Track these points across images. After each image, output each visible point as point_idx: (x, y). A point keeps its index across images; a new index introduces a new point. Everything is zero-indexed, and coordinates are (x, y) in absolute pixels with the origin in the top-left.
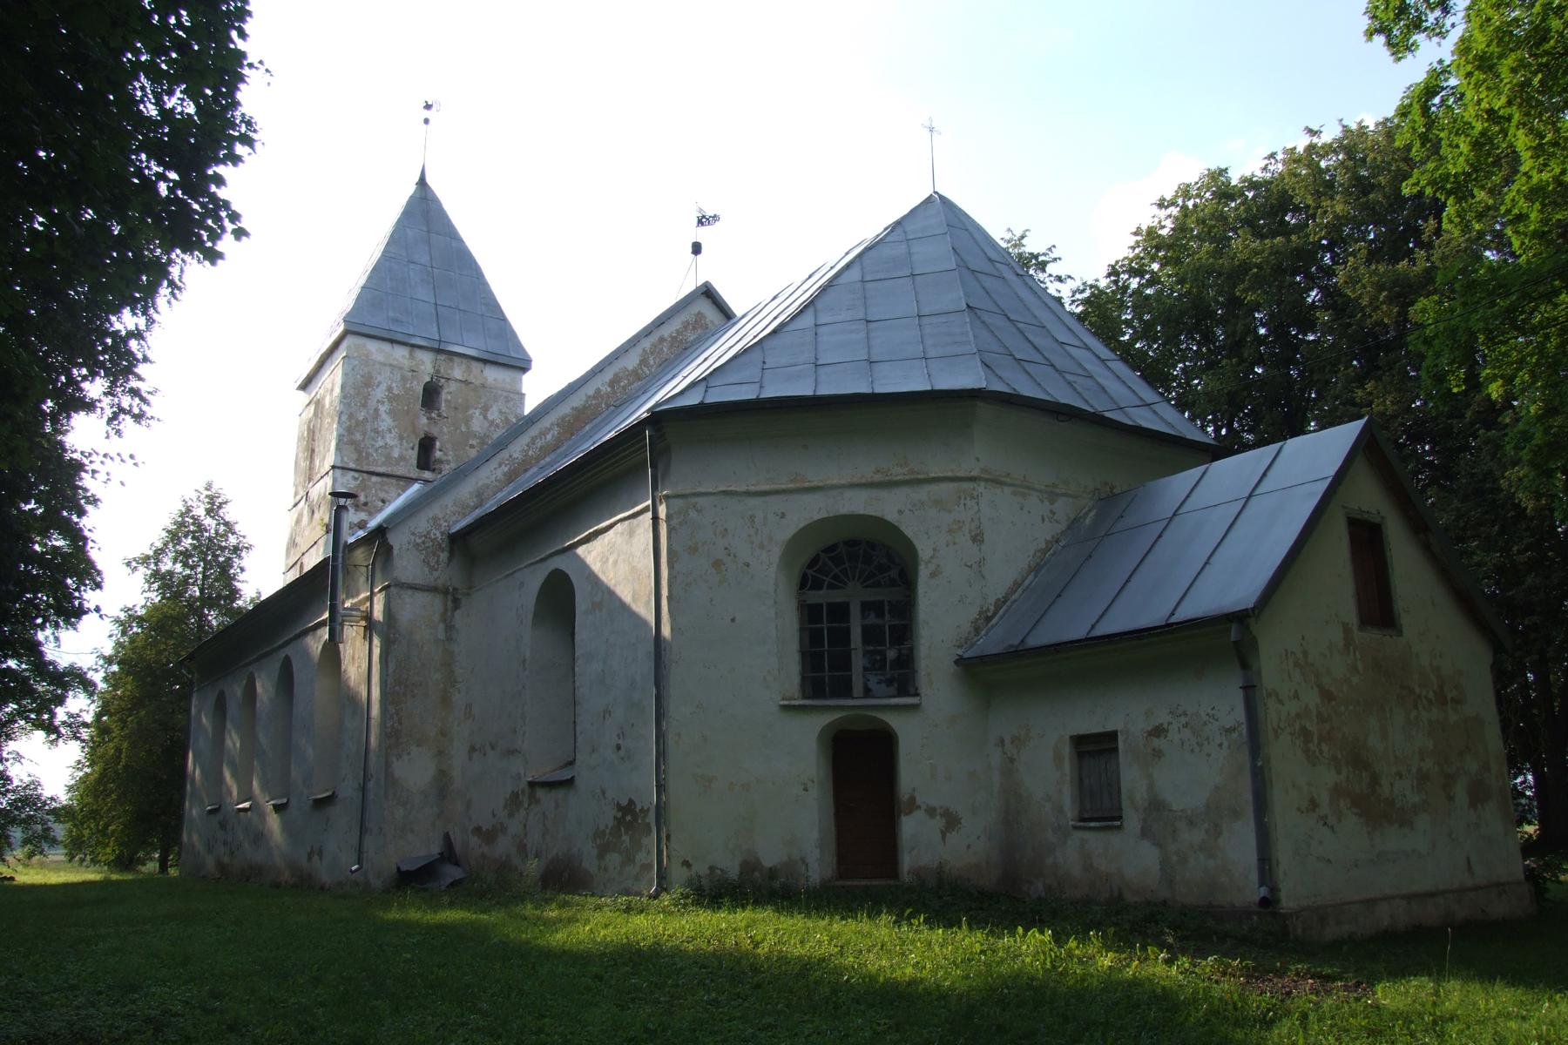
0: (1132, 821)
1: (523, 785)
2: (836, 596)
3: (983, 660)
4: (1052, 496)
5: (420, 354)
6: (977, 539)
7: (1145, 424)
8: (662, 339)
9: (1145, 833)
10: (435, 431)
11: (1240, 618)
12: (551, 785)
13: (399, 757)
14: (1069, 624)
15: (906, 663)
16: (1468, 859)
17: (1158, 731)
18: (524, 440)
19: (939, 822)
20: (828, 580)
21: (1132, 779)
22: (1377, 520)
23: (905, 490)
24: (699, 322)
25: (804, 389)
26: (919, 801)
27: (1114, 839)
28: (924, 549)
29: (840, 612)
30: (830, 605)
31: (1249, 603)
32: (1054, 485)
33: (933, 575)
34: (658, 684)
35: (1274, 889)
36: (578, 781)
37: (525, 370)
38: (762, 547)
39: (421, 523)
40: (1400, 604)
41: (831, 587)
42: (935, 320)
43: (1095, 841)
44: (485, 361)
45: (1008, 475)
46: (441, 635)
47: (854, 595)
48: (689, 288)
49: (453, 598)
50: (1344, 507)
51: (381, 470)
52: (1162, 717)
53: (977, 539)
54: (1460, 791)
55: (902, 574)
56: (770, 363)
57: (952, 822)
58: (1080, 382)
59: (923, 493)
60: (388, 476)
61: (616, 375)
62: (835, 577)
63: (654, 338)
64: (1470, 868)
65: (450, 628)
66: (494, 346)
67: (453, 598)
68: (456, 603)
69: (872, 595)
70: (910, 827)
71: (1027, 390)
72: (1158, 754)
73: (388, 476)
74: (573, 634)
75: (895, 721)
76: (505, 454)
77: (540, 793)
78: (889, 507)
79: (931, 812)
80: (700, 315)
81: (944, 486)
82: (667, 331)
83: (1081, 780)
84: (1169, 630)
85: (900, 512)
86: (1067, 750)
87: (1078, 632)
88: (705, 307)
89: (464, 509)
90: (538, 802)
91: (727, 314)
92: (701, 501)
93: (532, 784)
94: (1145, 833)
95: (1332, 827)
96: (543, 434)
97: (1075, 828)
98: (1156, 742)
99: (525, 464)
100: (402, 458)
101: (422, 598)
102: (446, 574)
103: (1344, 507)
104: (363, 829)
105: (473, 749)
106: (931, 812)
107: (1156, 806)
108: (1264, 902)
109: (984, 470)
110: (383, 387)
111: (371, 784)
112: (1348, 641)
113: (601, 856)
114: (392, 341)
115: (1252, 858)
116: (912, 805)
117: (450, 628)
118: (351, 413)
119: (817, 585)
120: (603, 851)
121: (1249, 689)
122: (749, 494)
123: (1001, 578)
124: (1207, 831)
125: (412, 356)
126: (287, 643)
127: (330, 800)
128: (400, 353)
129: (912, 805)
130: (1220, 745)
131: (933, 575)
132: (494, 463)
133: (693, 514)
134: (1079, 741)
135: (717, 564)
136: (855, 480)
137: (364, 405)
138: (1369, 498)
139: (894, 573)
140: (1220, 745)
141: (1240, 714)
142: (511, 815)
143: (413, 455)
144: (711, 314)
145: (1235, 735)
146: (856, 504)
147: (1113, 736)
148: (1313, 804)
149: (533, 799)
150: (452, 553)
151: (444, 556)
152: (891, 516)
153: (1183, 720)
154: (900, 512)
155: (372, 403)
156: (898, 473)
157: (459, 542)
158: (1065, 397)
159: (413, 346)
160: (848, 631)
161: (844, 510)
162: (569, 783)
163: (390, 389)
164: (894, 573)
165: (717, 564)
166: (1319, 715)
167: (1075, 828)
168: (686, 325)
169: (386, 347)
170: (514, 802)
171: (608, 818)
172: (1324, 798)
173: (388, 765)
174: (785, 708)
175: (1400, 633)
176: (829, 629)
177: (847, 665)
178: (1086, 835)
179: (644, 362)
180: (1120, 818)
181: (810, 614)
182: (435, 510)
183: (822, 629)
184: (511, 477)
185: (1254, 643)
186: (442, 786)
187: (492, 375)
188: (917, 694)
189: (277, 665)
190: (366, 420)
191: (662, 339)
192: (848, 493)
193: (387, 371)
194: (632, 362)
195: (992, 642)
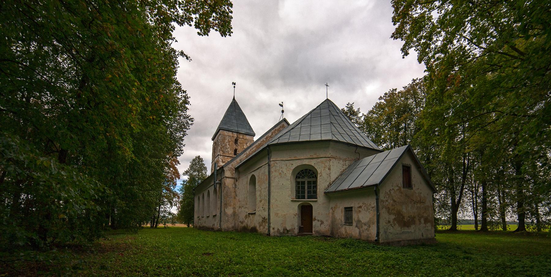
0: (354, 224)
1: (247, 214)
2: (303, 180)
3: (328, 192)
4: (345, 160)
5: (234, 133)
6: (329, 169)
7: (365, 146)
8: (276, 130)
9: (356, 226)
10: (237, 148)
11: (376, 185)
12: (252, 214)
13: (226, 208)
14: (345, 186)
15: (315, 192)
16: (422, 233)
17: (360, 207)
18: (249, 150)
19: (320, 223)
20: (301, 177)
21: (355, 216)
22: (409, 166)
23: (316, 159)
24: (283, 126)
25: (319, 138)
26: (316, 218)
27: (351, 227)
28: (319, 171)
29: (303, 183)
30: (301, 182)
31: (378, 181)
32: (346, 158)
33: (320, 176)
34: (269, 196)
35: (378, 238)
36: (256, 213)
37: (254, 136)
38: (288, 171)
39: (230, 166)
40: (413, 182)
41: (302, 178)
42: (324, 125)
43: (348, 227)
44: (246, 134)
45: (336, 157)
46: (234, 186)
47: (306, 180)
48: (281, 119)
49: (236, 180)
50: (402, 163)
51: (227, 155)
52: (361, 205)
53: (329, 169)
54: (422, 221)
55: (315, 175)
56: (292, 134)
57: (322, 223)
58: (353, 138)
59: (319, 160)
60: (229, 156)
61: (267, 137)
62: (303, 176)
63: (274, 130)
64: (423, 236)
65: (235, 185)
66: (248, 131)
67: (236, 180)
68: (237, 181)
69: (310, 180)
70: (314, 223)
71: (341, 139)
72: (360, 211)
73: (229, 156)
74: (255, 186)
75: (312, 204)
76: (245, 153)
77: (250, 215)
78: (312, 163)
79: (318, 221)
80: (283, 125)
81: (323, 159)
82: (277, 128)
83: (346, 216)
84: (362, 188)
85: (315, 164)
86: (343, 210)
87: (346, 188)
88: (284, 123)
89: (238, 163)
90: (250, 217)
91: (288, 124)
92: (277, 162)
93: (249, 214)
94: (356, 226)
95: (393, 227)
96: (253, 149)
97: (344, 225)
98: (360, 209)
99: (250, 154)
100: (231, 153)
101: (230, 179)
102: (235, 176)
103: (402, 163)
104: (221, 221)
105: (240, 207)
106: (318, 221)
107: (359, 221)
108: (376, 240)
109: (332, 156)
110: (227, 140)
111: (222, 213)
112: (399, 189)
113: (260, 227)
114: (229, 131)
115: (376, 232)
116: (315, 219)
117: (235, 185)
118: (84, 148)
119: (299, 178)
120: (260, 226)
121: (377, 200)
122: (286, 160)
123: (333, 177)
124: (368, 226)
125: (233, 134)
126: (209, 188)
127: (216, 215)
128: (230, 134)
129: (315, 219)
130: (371, 210)
131: (320, 176)
132: (243, 154)
133: (276, 164)
134: (346, 208)
135: (280, 174)
136: (306, 158)
137: (224, 143)
138: (408, 161)
139: (314, 175)
140: (371, 210)
141: (375, 204)
142: (246, 219)
143: (233, 153)
144: (286, 125)
145: (374, 208)
146: (306, 162)
147: (352, 208)
148: (389, 222)
149: (249, 216)
150: (236, 171)
151: (234, 172)
152: (313, 165)
153: (365, 205)
154: (315, 164)
155: (225, 143)
156: (315, 156)
157: (237, 169)
158: (348, 140)
159: (233, 132)
160: (305, 186)
161: (304, 163)
162: (255, 213)
163: (228, 140)
164: (314, 175)
165: (280, 174)
166: (392, 205)
167: (344, 225)
168: (280, 127)
169: (228, 132)
170: (246, 217)
171: (261, 220)
172: (392, 221)
173: (224, 210)
174: (292, 201)
175: (412, 189)
176: (311, 184)
177: (304, 193)
178: (347, 226)
179: (272, 134)
180: (352, 223)
181: (298, 183)
182: (233, 163)
183: (313, 184)
184: (246, 157)
185: (379, 190)
186: (234, 214)
187: (248, 137)
188: (317, 198)
189: (207, 191)
190: (224, 146)
191: (276, 130)
192: (305, 160)
193: (228, 137)
194: (270, 134)
195: (332, 189)
